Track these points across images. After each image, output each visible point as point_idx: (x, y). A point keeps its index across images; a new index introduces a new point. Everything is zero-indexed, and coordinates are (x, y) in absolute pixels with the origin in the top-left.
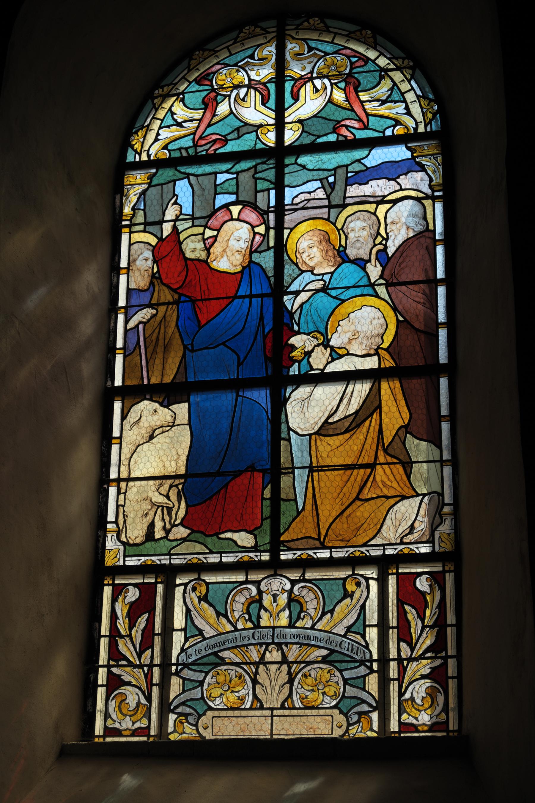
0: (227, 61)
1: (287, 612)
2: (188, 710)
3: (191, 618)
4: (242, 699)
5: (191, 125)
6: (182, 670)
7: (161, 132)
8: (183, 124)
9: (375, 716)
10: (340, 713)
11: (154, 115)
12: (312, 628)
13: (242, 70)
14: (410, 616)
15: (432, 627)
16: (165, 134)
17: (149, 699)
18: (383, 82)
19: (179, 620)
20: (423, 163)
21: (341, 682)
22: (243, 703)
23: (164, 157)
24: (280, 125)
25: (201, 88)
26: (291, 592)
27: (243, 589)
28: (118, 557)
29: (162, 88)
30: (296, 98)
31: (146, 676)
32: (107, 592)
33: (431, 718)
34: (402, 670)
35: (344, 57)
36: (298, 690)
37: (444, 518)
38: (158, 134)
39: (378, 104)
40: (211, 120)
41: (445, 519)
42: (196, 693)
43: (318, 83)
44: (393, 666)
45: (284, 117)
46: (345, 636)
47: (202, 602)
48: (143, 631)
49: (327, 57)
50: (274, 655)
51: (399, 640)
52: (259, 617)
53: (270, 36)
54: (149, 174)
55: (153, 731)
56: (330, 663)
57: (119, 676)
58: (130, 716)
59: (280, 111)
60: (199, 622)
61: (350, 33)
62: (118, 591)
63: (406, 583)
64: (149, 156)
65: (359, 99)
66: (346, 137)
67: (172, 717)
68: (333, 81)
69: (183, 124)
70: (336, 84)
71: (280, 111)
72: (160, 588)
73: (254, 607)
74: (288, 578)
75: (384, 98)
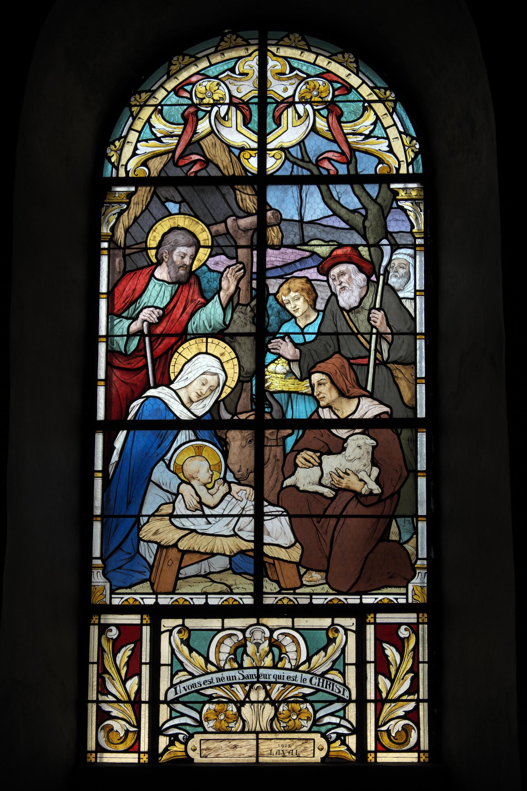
5: (170, 142)
7: (139, 145)
11: (132, 124)
13: (222, 84)
16: (143, 148)
20: (406, 207)
23: (142, 175)
28: (104, 593)
30: (278, 123)
35: (327, 82)
37: (418, 571)
38: (136, 148)
40: (192, 137)
41: (419, 573)
43: (300, 108)
52: (242, 660)
53: (251, 49)
59: (262, 135)
64: (127, 172)
66: (328, 170)
68: (315, 108)
69: (162, 139)
70: (318, 110)
71: (262, 135)
72: (146, 631)
75: (367, 132)
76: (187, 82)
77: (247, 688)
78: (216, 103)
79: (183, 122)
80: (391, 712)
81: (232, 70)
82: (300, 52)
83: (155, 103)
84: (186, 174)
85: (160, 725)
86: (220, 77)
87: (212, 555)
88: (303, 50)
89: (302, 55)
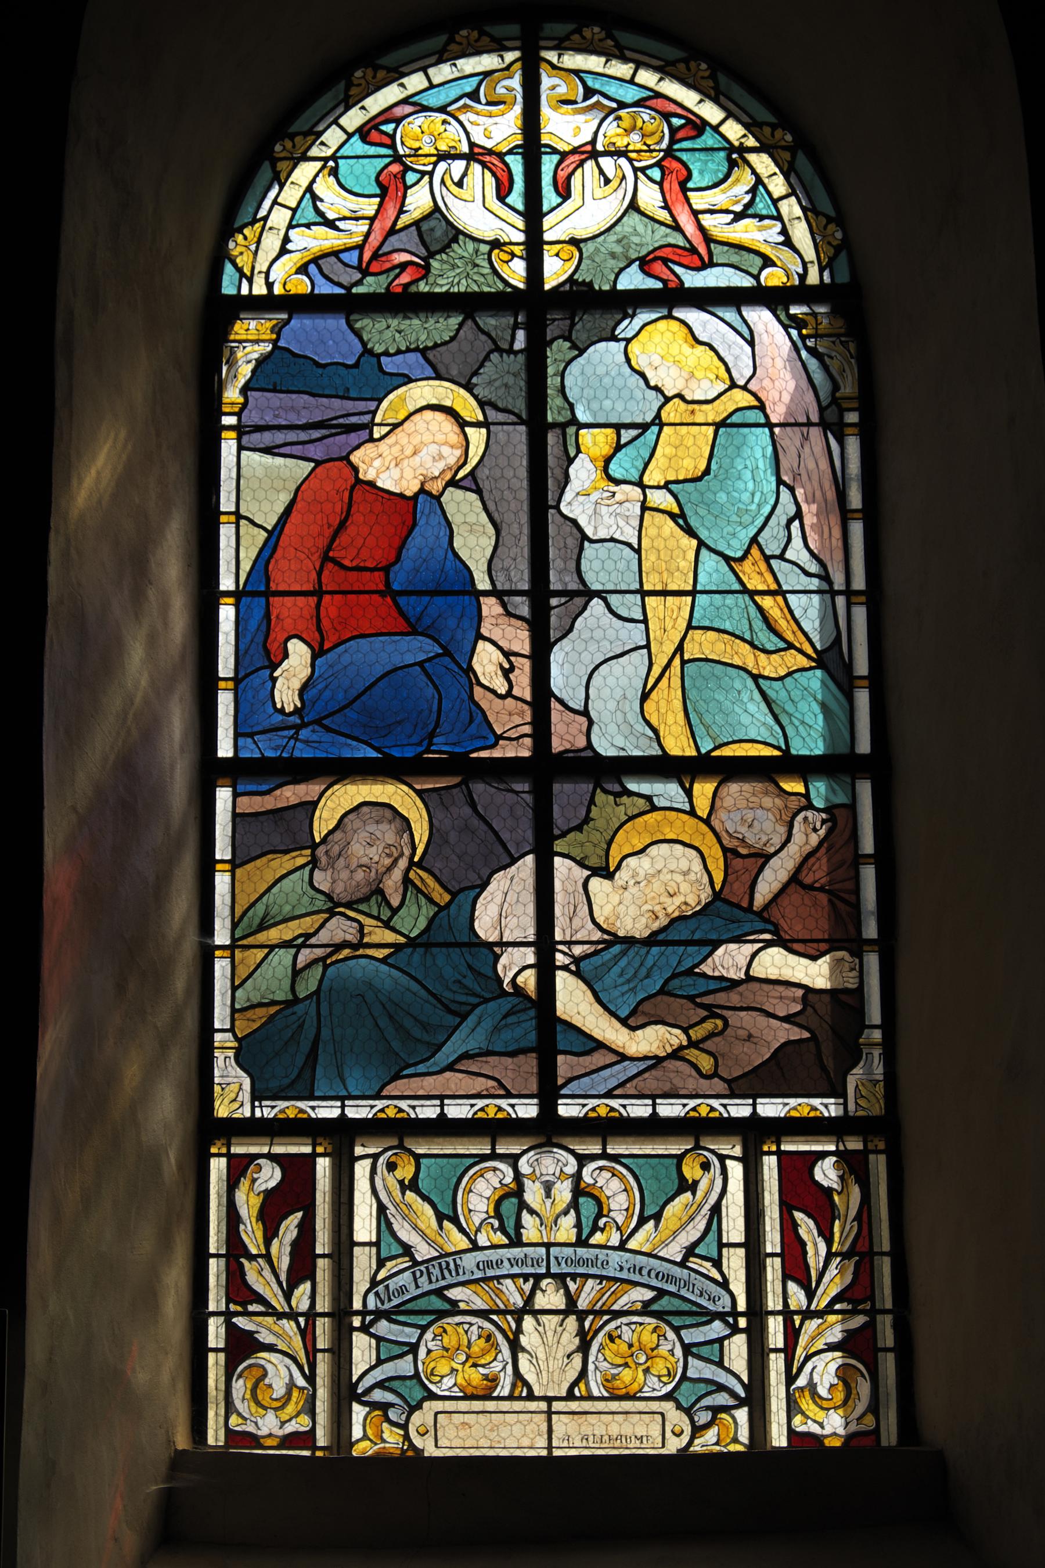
1: (572, 1216)
2: (390, 1397)
3: (389, 1225)
4: (493, 1380)
6: (372, 1323)
7: (292, 233)
9: (742, 1415)
10: (677, 1408)
12: (622, 1247)
14: (803, 1232)
15: (845, 1256)
16: (300, 239)
17: (311, 1379)
19: (364, 1228)
21: (679, 1352)
22: (496, 1387)
25: (372, 150)
26: (578, 1177)
27: (488, 1169)
28: (240, 1098)
29: (292, 137)
30: (564, 192)
31: (303, 1332)
32: (218, 1167)
33: (847, 1424)
34: (792, 1334)
35: (657, 116)
36: (600, 1362)
37: (865, 1051)
38: (286, 240)
39: (729, 221)
40: (397, 218)
42: (405, 1366)
43: (606, 162)
44: (775, 1327)
45: (540, 232)
46: (682, 1264)
47: (408, 1192)
48: (294, 1244)
49: (623, 113)
50: (550, 1298)
51: (786, 1277)
52: (519, 1225)
54: (274, 322)
55: (322, 1440)
56: (659, 1315)
57: (251, 1334)
58: (276, 1409)
59: (533, 215)
60: (405, 1233)
61: (668, 63)
63: (797, 1172)
64: (270, 285)
65: (690, 205)
67: (359, 1412)
68: (637, 164)
69: (337, 223)
70: (643, 170)
71: (533, 215)
72: (323, 1165)
73: (512, 1203)
74: (572, 1152)
75: (738, 208)
76: (386, 115)
77: (527, 1287)
78: (442, 157)
79: (378, 191)
80: (819, 1334)
81: (474, 96)
82: (603, 59)
83: (323, 155)
84: (388, 288)
85: (354, 1379)
86: (449, 109)
87: (475, 281)
88: (609, 56)
89: (608, 65)
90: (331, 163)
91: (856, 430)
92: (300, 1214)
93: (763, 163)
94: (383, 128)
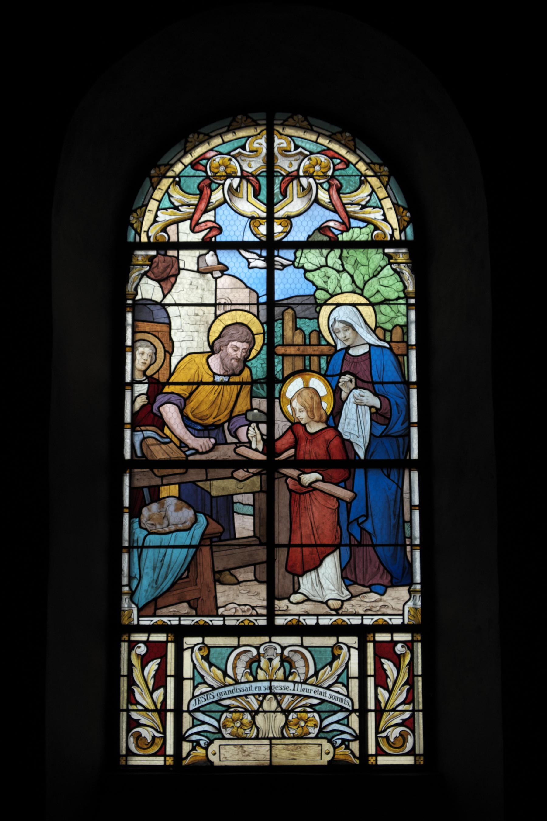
0: (220, 149)
7: (159, 213)
8: (180, 208)
13: (233, 160)
14: (385, 666)
18: (363, 187)
19: (187, 671)
24: (270, 219)
49: (312, 156)
51: (376, 687)
52: (257, 673)
59: (270, 205)
62: (132, 645)
64: (149, 238)
65: (341, 201)
68: (318, 181)
70: (321, 184)
71: (270, 205)
75: (363, 203)
76: (202, 156)
77: (261, 698)
90: (177, 179)
91: (414, 307)
92: (158, 661)
93: (374, 181)
94: (201, 162)
